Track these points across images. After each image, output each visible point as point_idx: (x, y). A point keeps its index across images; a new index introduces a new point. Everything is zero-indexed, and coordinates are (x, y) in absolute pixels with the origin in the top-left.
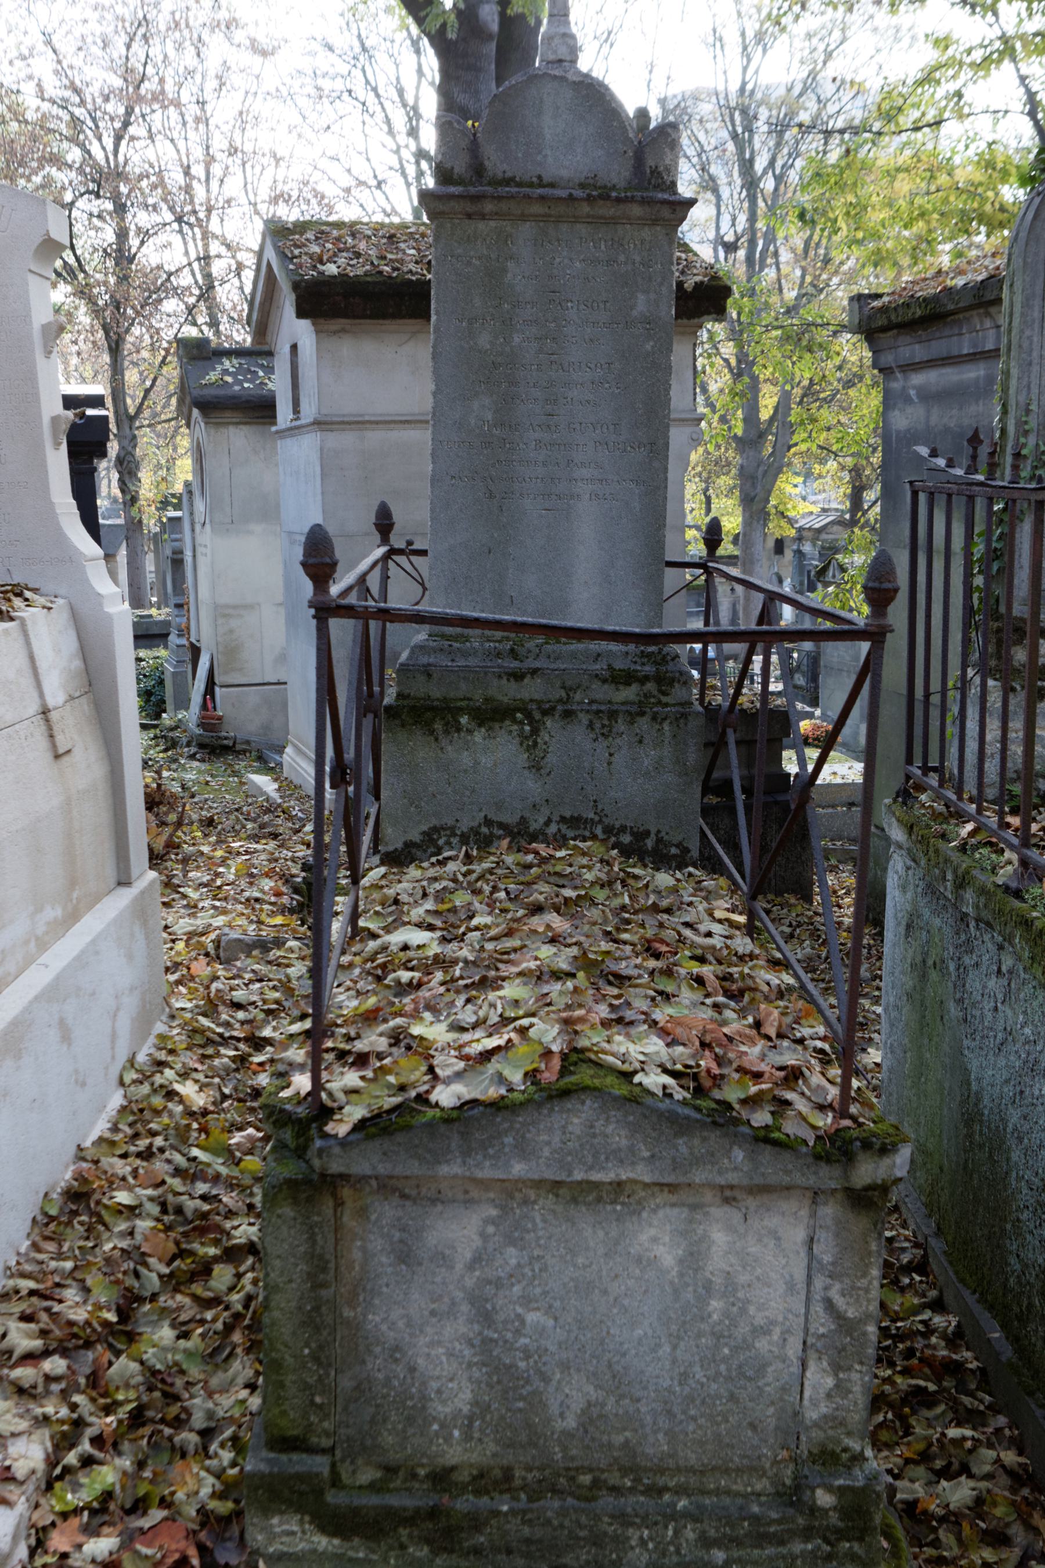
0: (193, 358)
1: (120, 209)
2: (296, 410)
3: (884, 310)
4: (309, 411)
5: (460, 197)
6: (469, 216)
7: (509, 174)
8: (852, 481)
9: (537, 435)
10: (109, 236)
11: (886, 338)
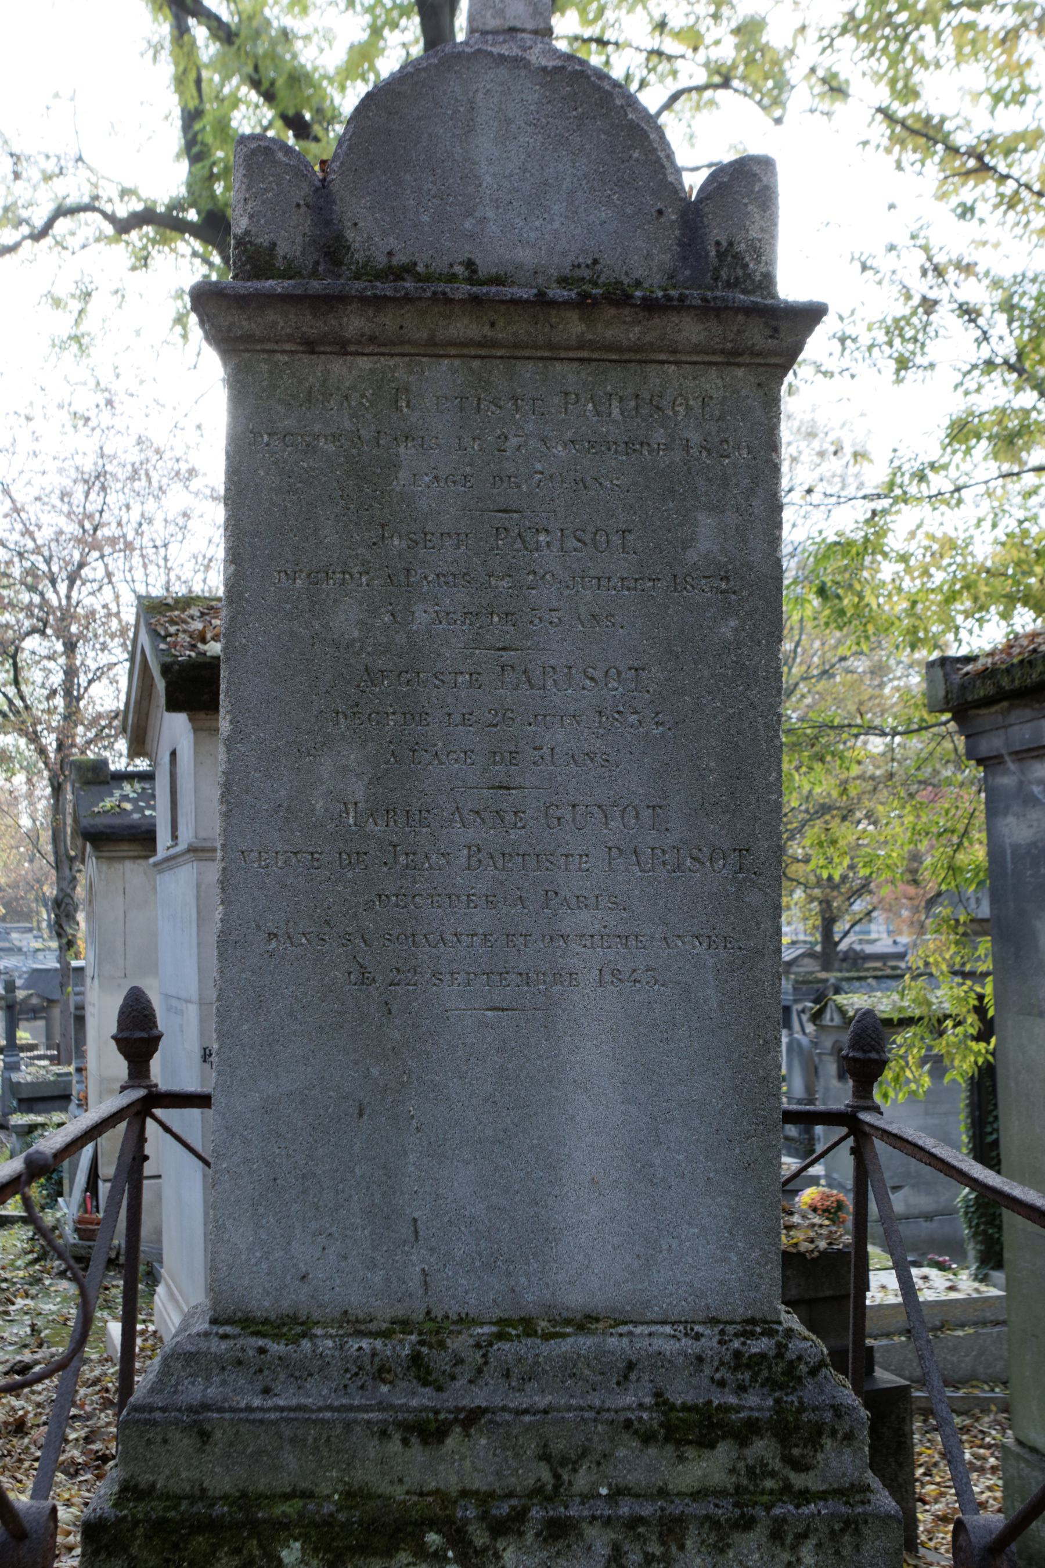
0: (88, 783)
1: (71, 647)
2: (175, 837)
3: (987, 674)
4: (186, 836)
5: (286, 298)
6: (311, 346)
7: (400, 259)
8: (822, 912)
9: (470, 835)
10: (57, 679)
11: (988, 716)
